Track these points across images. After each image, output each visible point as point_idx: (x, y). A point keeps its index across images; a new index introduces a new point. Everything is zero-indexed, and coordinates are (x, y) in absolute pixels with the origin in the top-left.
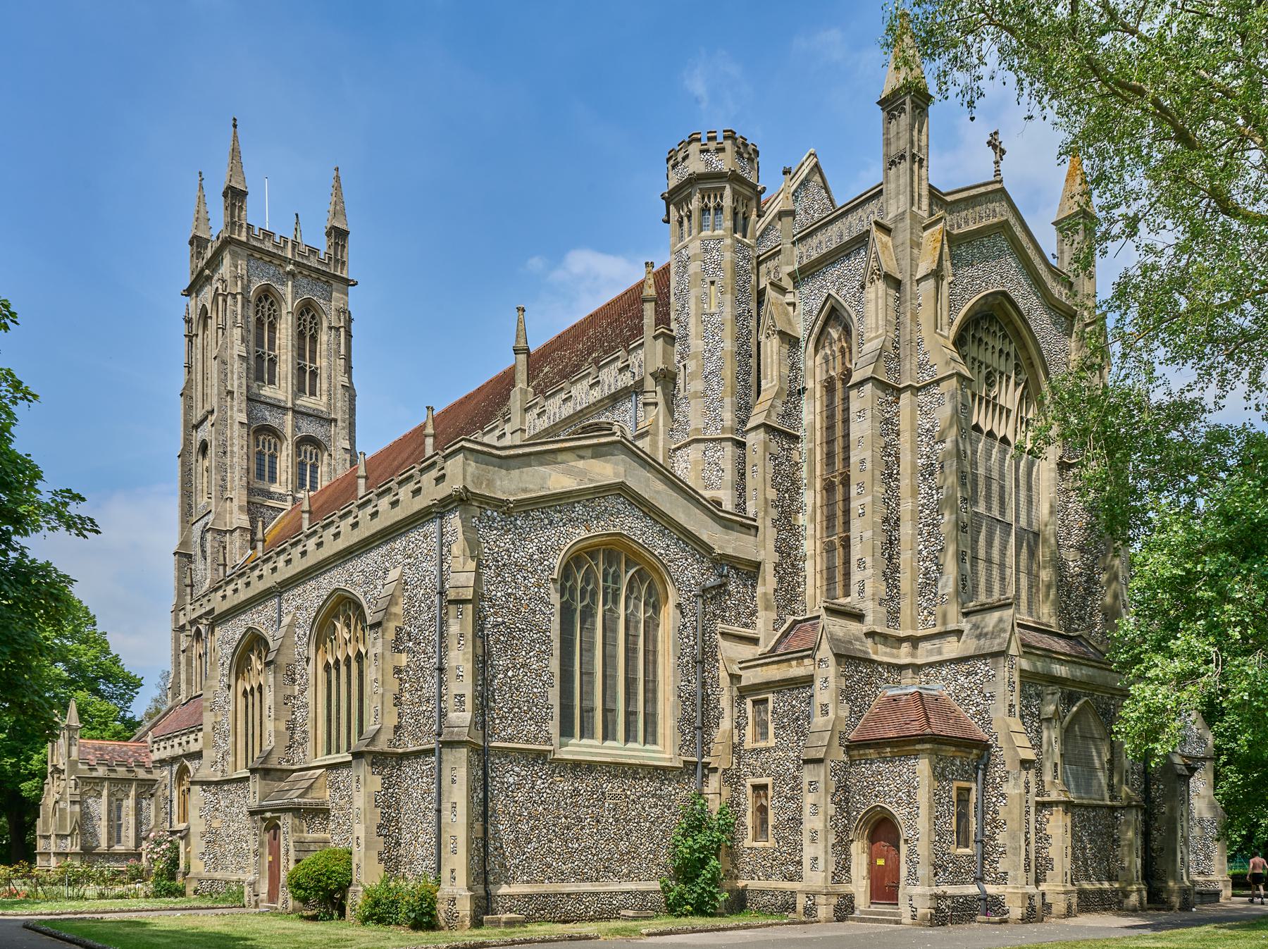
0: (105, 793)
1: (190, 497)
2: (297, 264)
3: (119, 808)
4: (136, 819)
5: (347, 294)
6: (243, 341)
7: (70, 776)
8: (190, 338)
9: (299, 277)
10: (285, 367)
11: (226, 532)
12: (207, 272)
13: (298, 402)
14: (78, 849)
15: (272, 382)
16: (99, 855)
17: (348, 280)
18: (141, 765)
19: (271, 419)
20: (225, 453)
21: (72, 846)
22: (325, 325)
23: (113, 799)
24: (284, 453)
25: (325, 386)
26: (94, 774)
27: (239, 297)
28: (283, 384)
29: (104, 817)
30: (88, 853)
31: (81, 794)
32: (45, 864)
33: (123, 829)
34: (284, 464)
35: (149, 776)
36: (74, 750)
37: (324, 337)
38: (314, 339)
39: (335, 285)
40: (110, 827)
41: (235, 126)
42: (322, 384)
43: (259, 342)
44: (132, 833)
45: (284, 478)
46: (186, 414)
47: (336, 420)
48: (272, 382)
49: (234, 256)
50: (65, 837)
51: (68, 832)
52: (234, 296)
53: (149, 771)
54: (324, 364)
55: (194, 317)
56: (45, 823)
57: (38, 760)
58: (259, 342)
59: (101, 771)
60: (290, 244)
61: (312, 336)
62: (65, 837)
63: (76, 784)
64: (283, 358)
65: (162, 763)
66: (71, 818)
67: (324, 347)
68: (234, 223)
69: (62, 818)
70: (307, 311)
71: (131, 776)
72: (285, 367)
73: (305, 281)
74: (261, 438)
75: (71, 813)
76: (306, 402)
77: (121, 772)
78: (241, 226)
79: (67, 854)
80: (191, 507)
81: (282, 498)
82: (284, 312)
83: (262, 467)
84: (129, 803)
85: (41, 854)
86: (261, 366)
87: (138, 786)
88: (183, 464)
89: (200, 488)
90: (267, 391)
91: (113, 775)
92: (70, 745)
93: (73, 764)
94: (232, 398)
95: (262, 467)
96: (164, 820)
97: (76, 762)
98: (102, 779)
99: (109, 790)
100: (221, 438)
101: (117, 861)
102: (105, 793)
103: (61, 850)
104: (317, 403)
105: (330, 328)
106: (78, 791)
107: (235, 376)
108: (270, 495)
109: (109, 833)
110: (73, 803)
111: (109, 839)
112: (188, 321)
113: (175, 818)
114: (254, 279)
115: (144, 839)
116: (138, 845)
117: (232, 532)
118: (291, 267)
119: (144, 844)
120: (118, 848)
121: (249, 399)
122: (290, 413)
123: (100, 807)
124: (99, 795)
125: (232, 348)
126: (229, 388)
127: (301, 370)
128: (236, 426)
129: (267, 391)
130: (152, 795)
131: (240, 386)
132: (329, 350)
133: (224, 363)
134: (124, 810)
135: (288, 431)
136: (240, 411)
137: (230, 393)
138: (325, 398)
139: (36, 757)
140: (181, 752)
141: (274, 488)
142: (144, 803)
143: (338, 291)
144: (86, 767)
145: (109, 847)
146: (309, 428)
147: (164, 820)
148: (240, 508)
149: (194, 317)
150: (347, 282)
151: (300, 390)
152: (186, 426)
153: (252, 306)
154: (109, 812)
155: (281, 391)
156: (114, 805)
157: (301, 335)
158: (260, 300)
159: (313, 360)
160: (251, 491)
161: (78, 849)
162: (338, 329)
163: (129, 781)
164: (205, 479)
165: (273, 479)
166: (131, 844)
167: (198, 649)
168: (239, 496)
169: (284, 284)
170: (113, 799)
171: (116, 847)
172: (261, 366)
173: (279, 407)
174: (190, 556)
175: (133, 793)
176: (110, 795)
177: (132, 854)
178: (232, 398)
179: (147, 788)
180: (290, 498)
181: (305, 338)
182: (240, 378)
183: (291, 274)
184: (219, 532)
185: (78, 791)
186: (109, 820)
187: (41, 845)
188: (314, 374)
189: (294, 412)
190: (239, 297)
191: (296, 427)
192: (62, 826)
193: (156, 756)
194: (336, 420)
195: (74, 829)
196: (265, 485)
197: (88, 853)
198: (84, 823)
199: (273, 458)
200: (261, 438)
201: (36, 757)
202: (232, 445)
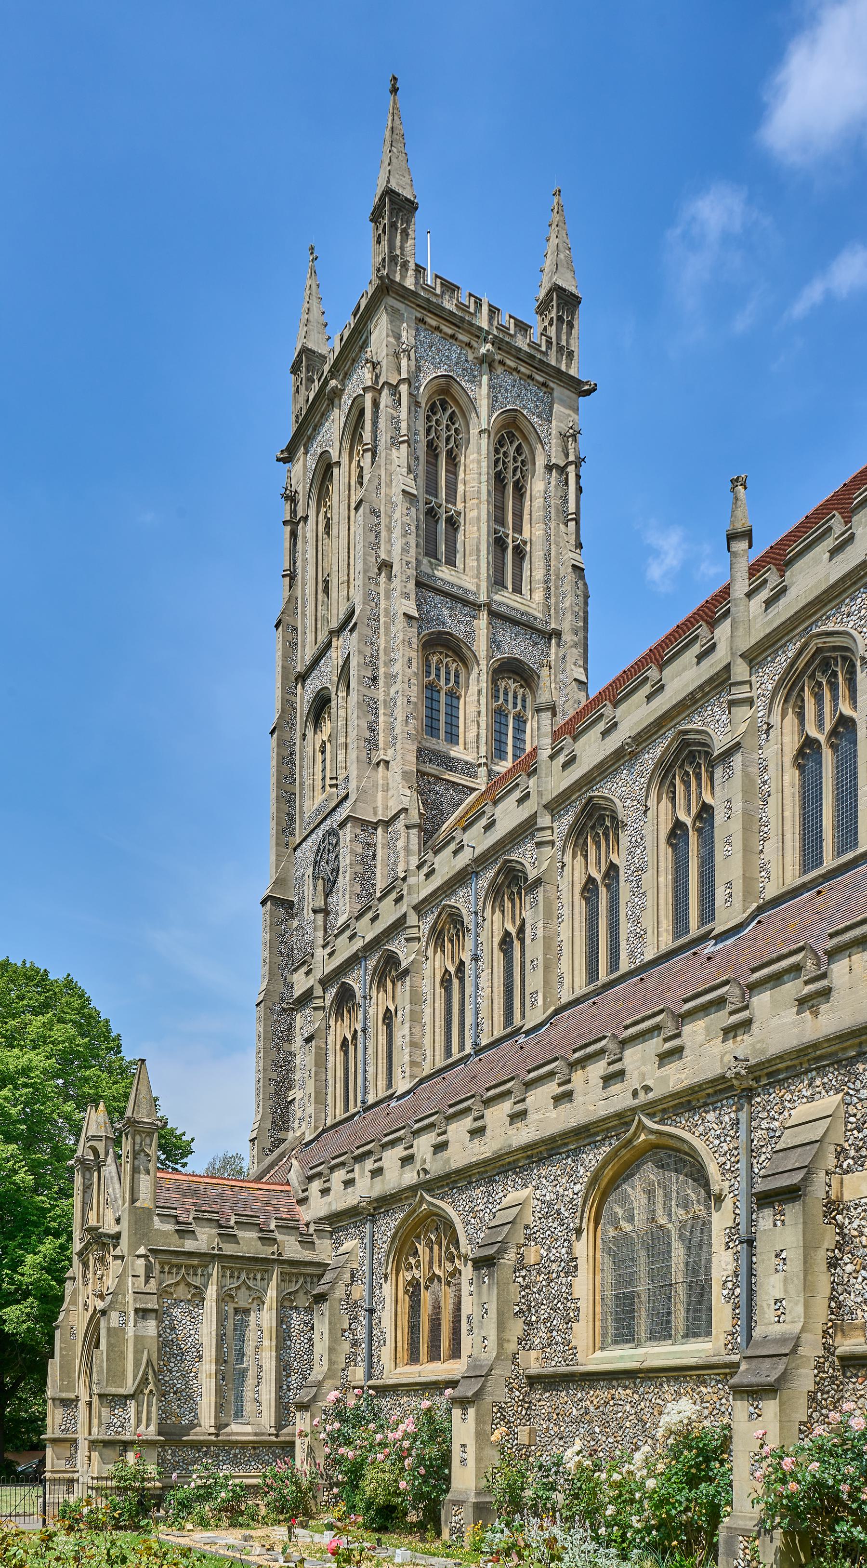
0: (212, 1292)
1: (290, 801)
2: (498, 343)
3: (241, 1329)
4: (279, 1359)
5: (576, 410)
6: (410, 471)
7: (133, 1246)
8: (294, 524)
9: (500, 370)
10: (475, 532)
11: (375, 825)
12: (333, 383)
13: (497, 597)
14: (150, 1432)
15: (451, 562)
16: (197, 1445)
17: (579, 382)
18: (290, 1226)
19: (452, 622)
20: (374, 679)
21: (140, 1423)
22: (540, 462)
23: (229, 1308)
24: (473, 689)
25: (539, 574)
26: (189, 1245)
27: (404, 388)
28: (471, 562)
29: (209, 1352)
30: (173, 1438)
31: (163, 1293)
32: (62, 1465)
33: (250, 1382)
34: (472, 709)
35: (305, 1255)
36: (145, 1183)
37: (538, 485)
38: (520, 490)
39: (559, 391)
40: (221, 1377)
41: (394, 90)
42: (535, 570)
43: (432, 487)
44: (268, 1392)
45: (471, 735)
46: (285, 657)
47: (558, 634)
48: (451, 562)
49: (395, 316)
50: (121, 1400)
51: (129, 1387)
52: (394, 389)
53: (307, 1243)
54: (539, 532)
55: (302, 490)
56: (67, 1370)
57: (34, 1266)
58: (432, 487)
59: (204, 1239)
60: (485, 309)
61: (516, 484)
62: (121, 1400)
63: (149, 1268)
64: (472, 514)
65: (338, 1222)
66: (138, 1352)
67: (539, 502)
68: (393, 259)
69: (116, 1355)
70: (511, 434)
71: (267, 1252)
72: (475, 532)
73: (509, 379)
74: (434, 659)
75: (138, 1338)
76: (506, 598)
77: (248, 1242)
78: (405, 265)
79: (126, 1445)
80: (292, 820)
81: (469, 769)
82: (474, 431)
83: (437, 715)
84: (265, 1318)
85: (54, 1441)
86: (437, 528)
87: (285, 1278)
88: (281, 744)
89: (308, 782)
90: (444, 573)
91: (229, 1249)
92: (135, 1170)
93: (141, 1219)
94: (389, 578)
95: (437, 715)
96: (351, 1359)
97: (147, 1214)
98: (207, 1258)
99: (220, 1287)
100: (368, 651)
101: (235, 1462)
102: (212, 1292)
103: (111, 1436)
104: (531, 602)
105: (549, 468)
106: (153, 1286)
107: (397, 532)
108: (449, 763)
109: (219, 1392)
110: (142, 1313)
111: (220, 1407)
112: (291, 498)
113: (385, 1354)
114: (426, 365)
115: (303, 1407)
116: (282, 1419)
117: (387, 824)
118: (489, 346)
119: (301, 1422)
120: (239, 1430)
121: (419, 584)
122: (484, 615)
123: (204, 1329)
124: (199, 1296)
125: (389, 484)
126: (383, 556)
127: (499, 543)
128: (400, 621)
129: (444, 573)
130: (321, 1298)
131: (405, 550)
132: (547, 508)
133: (375, 513)
134: (251, 1335)
135: (481, 646)
136: (407, 596)
137: (386, 566)
138: (539, 596)
139: (29, 1259)
140: (410, 1177)
141: (457, 752)
142: (296, 1321)
143: (563, 403)
144: (170, 1227)
145: (220, 1426)
146: (516, 646)
147: (351, 1359)
148: (405, 775)
149: (302, 490)
150: (580, 389)
151: (498, 582)
152: (285, 677)
153: (422, 414)
154: (221, 1339)
155: (470, 573)
156: (230, 1324)
157: (499, 480)
158: (433, 409)
159: (518, 528)
160: (422, 754)
161: (150, 1432)
162: (562, 470)
163: (261, 1265)
164: (319, 766)
165: (453, 737)
166: (267, 1420)
167: (339, 1031)
168: (402, 756)
169: (474, 380)
170: (229, 1308)
171: (234, 1428)
172: (437, 528)
173: (466, 603)
174: (291, 904)
175: (272, 1294)
176: (225, 1297)
177: (268, 1445)
178: (389, 578)
179: (307, 1284)
180: (482, 771)
181: (508, 485)
182: (405, 534)
183: (486, 361)
184: (364, 824)
185: (153, 1286)
186: (220, 1360)
187: (55, 1422)
188: (519, 553)
189: (493, 614)
190: (404, 388)
191: (494, 643)
192: (115, 1374)
193: (318, 1207)
194: (558, 634)
195: (145, 1381)
196: (441, 745)
197: (173, 1438)
198: (167, 1363)
199: (453, 696)
200: (434, 659)
201: (29, 1259)
202: (390, 662)
